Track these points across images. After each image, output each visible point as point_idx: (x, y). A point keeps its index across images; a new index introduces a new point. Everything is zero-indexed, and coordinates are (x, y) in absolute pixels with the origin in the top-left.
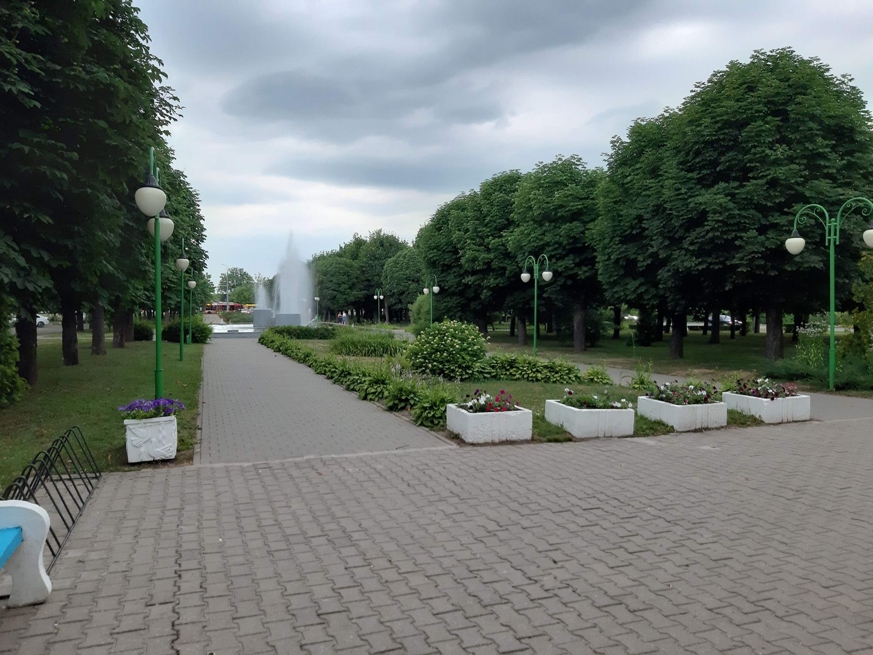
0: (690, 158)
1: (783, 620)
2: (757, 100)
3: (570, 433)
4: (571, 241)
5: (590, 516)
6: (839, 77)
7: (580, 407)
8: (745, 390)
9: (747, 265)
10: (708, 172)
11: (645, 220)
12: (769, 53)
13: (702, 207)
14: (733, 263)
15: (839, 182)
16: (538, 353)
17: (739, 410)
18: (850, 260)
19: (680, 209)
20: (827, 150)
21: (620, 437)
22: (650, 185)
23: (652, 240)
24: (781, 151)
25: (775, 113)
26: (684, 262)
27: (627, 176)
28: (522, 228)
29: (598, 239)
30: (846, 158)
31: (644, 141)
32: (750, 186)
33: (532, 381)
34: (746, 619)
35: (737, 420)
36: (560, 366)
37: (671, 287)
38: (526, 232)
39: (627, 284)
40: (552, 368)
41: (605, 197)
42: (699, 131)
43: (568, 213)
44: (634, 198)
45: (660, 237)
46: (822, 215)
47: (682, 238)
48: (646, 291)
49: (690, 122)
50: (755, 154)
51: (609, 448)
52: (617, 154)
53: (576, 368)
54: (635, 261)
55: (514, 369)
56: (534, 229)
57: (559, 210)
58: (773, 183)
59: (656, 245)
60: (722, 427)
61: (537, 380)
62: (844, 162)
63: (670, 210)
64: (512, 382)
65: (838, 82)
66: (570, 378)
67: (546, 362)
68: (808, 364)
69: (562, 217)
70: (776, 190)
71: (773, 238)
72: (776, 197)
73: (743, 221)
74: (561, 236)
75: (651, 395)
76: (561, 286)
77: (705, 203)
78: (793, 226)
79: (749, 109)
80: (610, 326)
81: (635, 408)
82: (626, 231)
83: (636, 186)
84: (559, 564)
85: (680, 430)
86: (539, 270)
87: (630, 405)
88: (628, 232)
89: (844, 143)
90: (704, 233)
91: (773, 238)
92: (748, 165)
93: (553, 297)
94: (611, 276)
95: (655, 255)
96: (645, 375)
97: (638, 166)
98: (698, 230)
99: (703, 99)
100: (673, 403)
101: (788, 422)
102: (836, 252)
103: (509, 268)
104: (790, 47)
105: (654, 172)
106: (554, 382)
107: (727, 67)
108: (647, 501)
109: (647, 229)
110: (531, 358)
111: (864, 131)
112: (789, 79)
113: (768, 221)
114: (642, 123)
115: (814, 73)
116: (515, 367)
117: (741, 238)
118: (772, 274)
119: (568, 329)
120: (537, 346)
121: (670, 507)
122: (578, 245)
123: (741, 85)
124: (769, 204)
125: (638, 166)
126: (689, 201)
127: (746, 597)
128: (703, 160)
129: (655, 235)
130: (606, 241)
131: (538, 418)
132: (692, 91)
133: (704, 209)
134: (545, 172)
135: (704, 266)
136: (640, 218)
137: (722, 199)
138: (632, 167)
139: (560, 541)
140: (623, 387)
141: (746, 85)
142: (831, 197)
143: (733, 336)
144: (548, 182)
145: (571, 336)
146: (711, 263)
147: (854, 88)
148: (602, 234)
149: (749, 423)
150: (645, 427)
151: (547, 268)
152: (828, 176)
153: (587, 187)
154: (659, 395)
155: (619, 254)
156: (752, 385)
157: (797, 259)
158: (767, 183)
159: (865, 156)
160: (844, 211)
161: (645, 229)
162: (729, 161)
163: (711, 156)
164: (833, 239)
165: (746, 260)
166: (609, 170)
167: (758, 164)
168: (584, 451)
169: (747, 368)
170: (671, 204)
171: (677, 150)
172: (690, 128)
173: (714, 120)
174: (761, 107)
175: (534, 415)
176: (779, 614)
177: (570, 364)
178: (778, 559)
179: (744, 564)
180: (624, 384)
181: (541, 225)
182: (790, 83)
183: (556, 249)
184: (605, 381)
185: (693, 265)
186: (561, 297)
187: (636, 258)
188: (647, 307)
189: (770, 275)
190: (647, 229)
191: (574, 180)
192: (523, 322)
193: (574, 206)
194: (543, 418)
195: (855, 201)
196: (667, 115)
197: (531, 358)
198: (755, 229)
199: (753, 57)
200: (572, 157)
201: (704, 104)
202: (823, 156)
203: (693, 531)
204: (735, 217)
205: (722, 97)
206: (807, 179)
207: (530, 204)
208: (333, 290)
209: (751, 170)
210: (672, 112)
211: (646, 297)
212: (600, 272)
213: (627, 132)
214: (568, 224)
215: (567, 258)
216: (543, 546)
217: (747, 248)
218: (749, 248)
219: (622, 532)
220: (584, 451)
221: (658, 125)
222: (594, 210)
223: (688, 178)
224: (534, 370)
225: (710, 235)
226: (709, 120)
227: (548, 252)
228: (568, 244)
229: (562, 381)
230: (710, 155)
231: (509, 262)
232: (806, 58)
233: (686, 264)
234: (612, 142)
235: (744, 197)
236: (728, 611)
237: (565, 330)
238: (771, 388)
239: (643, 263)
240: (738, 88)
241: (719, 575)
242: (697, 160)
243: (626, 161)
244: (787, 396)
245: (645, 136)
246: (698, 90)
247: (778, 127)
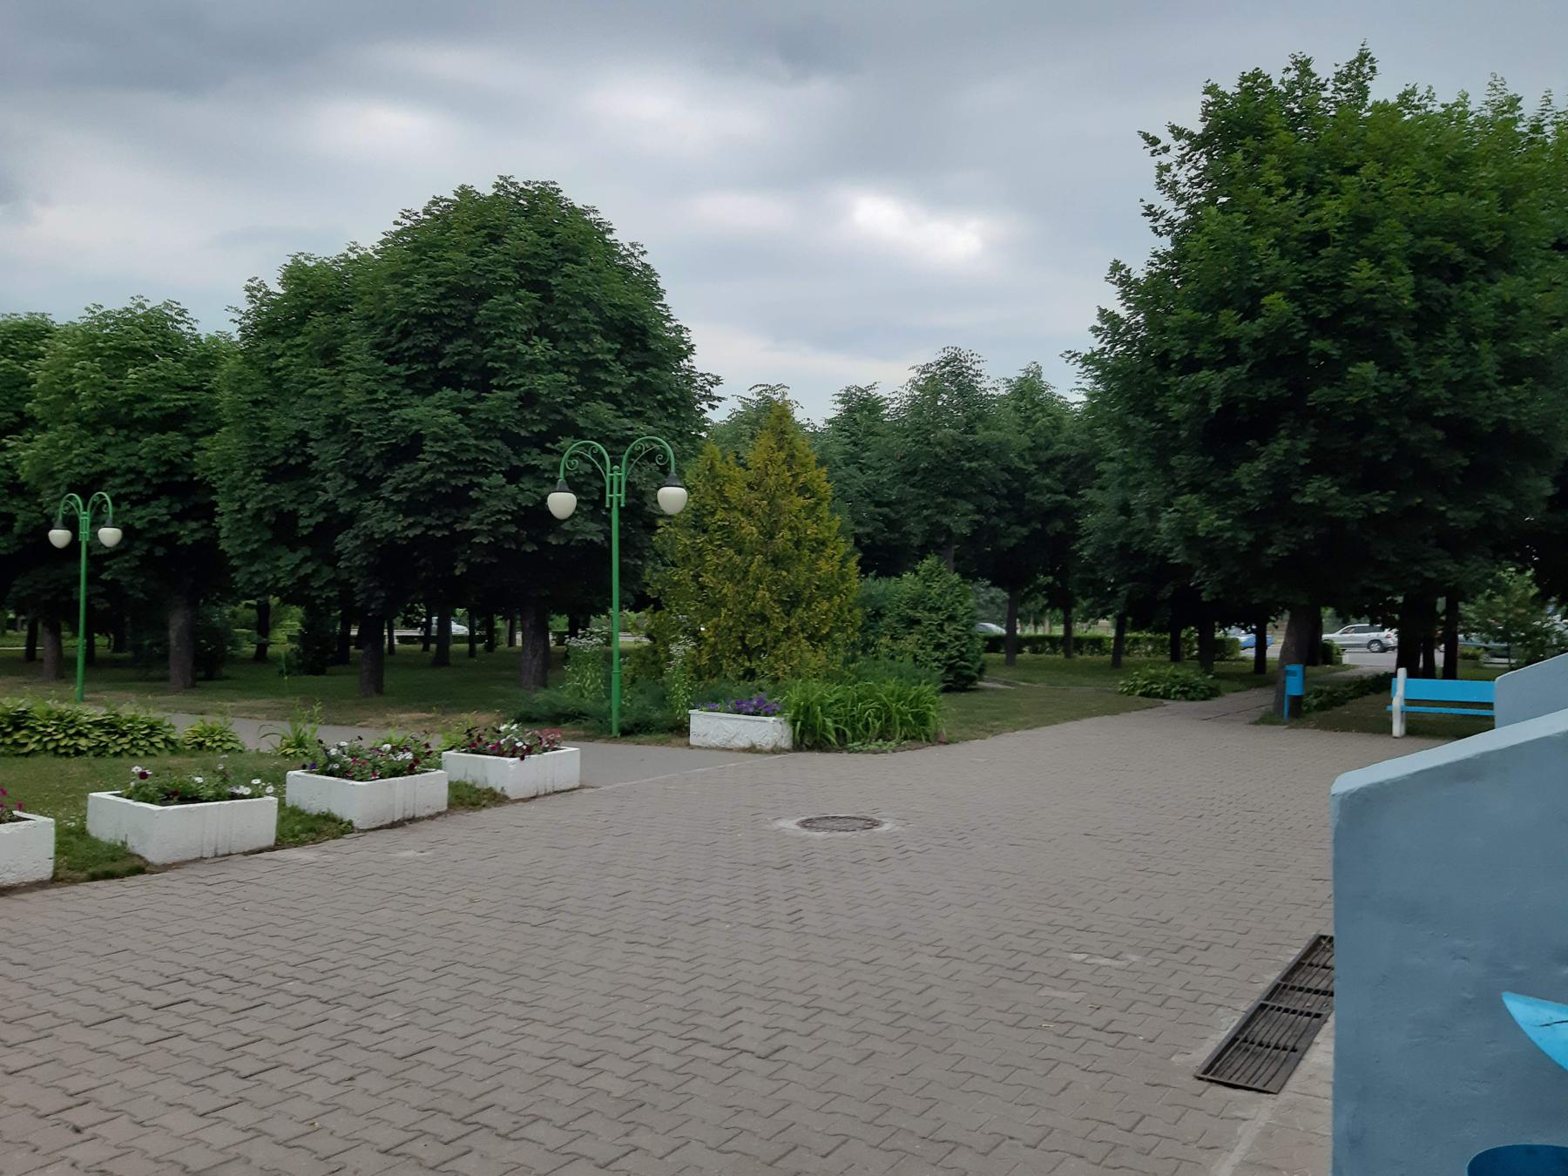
0: (392, 339)
1: (508, 1139)
2: (502, 258)
3: (140, 858)
4: (163, 469)
5: (168, 1020)
6: (627, 246)
7: (163, 802)
8: (479, 745)
9: (489, 533)
10: (425, 368)
11: (312, 440)
12: (522, 185)
13: (415, 427)
14: (465, 528)
15: (626, 409)
16: (86, 696)
17: (469, 782)
18: (643, 531)
19: (375, 428)
20: (609, 357)
21: (246, 854)
22: (321, 378)
23: (324, 479)
24: (540, 349)
25: (534, 286)
26: (382, 522)
27: (279, 357)
28: (51, 434)
29: (221, 469)
30: (635, 373)
31: (311, 297)
32: (494, 399)
33: (67, 755)
34: (635, 1049)
35: (466, 798)
36: (130, 721)
37: (360, 567)
38: (62, 443)
39: (278, 558)
40: (112, 726)
41: (235, 390)
42: (408, 294)
43: (157, 414)
44: (293, 400)
45: (339, 474)
46: (601, 458)
47: (380, 480)
48: (315, 572)
49: (394, 275)
50: (501, 348)
51: (222, 878)
52: (259, 313)
53: (167, 724)
54: (294, 515)
55: (24, 732)
56: (80, 440)
57: (137, 406)
58: (529, 399)
59: (332, 489)
60: (439, 814)
61: (78, 753)
62: (633, 379)
63: (359, 426)
64: (17, 760)
65: (624, 253)
66: (152, 744)
67: (98, 713)
68: (582, 696)
69: (141, 420)
70: (534, 412)
71: (529, 490)
72: (534, 422)
73: (481, 458)
74: (141, 458)
75: (312, 767)
77: (420, 421)
78: (558, 472)
79: (490, 271)
80: (249, 638)
81: (280, 795)
82: (276, 458)
83: (295, 377)
84: (87, 1134)
85: (365, 828)
86: (92, 525)
87: (270, 789)
88: (281, 461)
89: (634, 350)
90: (417, 473)
91: (529, 490)
92: (490, 364)
93: (124, 580)
94: (245, 543)
95: (329, 507)
96: (307, 730)
97: (299, 340)
98: (407, 467)
99: (415, 241)
100: (352, 778)
101: (547, 795)
102: (621, 517)
103: (21, 517)
104: (554, 183)
105: (329, 355)
106: (116, 754)
107: (456, 193)
108: (286, 971)
109: (316, 458)
110: (64, 707)
111: (660, 335)
112: (552, 235)
113: (522, 461)
114: (307, 262)
115: (590, 233)
116: (27, 728)
117: (479, 485)
118: (529, 550)
119: (158, 645)
120: (86, 680)
121: (330, 974)
122: (179, 479)
123: (478, 228)
124: (523, 433)
125: (299, 340)
126: (391, 414)
127: (449, 1114)
128: (415, 346)
129: (332, 470)
130: (239, 473)
131: (70, 832)
132: (396, 223)
133: (417, 431)
134: (107, 326)
135: (418, 531)
136: (303, 437)
137: (447, 418)
138: (289, 341)
139: (94, 1083)
140: (262, 756)
141: (486, 231)
142: (614, 431)
143: (472, 652)
144: (111, 348)
145: (164, 657)
146: (429, 527)
147: (647, 266)
148: (227, 460)
149: (484, 802)
150: (298, 827)
151: (109, 522)
152: (610, 398)
153: (199, 367)
154: (326, 765)
155: (262, 502)
156: (492, 737)
157: (566, 526)
158: (520, 398)
159: (663, 374)
160: (632, 456)
161: (311, 458)
162: (459, 354)
163: (429, 341)
164: (616, 498)
165: (488, 524)
166: (242, 340)
167: (504, 365)
168: (168, 891)
169: (489, 707)
170: (358, 417)
171: (371, 323)
172: (392, 286)
173: (432, 280)
174: (508, 271)
175: (57, 826)
176: (502, 1131)
177: (155, 715)
178: (509, 1032)
179: (453, 1053)
180: (265, 748)
181: (97, 432)
182: (556, 241)
183: (129, 483)
184: (228, 745)
185: (399, 528)
186: (143, 580)
187: (295, 511)
188: (318, 602)
189: (525, 552)
190: (316, 458)
191: (171, 351)
192: (56, 632)
193: (169, 401)
194: (82, 833)
195: (648, 440)
196: (353, 256)
197: (64, 707)
198: (501, 472)
199: (497, 185)
200: (167, 305)
201: (415, 250)
202: (602, 366)
203: (370, 1011)
204: (469, 450)
205: (447, 244)
206: (580, 399)
207: (71, 387)
209: (495, 372)
210: (362, 253)
211: (315, 584)
212: (223, 533)
213: (279, 274)
214: (156, 435)
215: (154, 503)
216: (50, 1101)
217: (488, 504)
218: (493, 504)
219: (230, 1040)
220: (168, 891)
221: (338, 272)
222: (214, 412)
223: (390, 375)
224: (71, 732)
225: (428, 477)
226: (424, 279)
227: (113, 487)
228: (156, 475)
229: (134, 751)
230: (426, 338)
231: (23, 504)
232: (578, 205)
233: (385, 526)
234: (248, 289)
235: (484, 417)
236: (417, 1148)
237: (151, 646)
238: (521, 740)
239: (307, 522)
240: (472, 233)
241: (407, 1084)
242: (404, 345)
243: (276, 327)
244: (545, 750)
245: (312, 288)
246: (408, 223)
247: (537, 309)
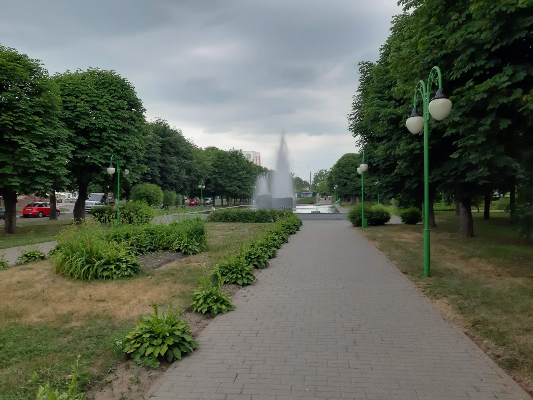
76: (487, 134)
151: (413, 111)
208: (344, 178)
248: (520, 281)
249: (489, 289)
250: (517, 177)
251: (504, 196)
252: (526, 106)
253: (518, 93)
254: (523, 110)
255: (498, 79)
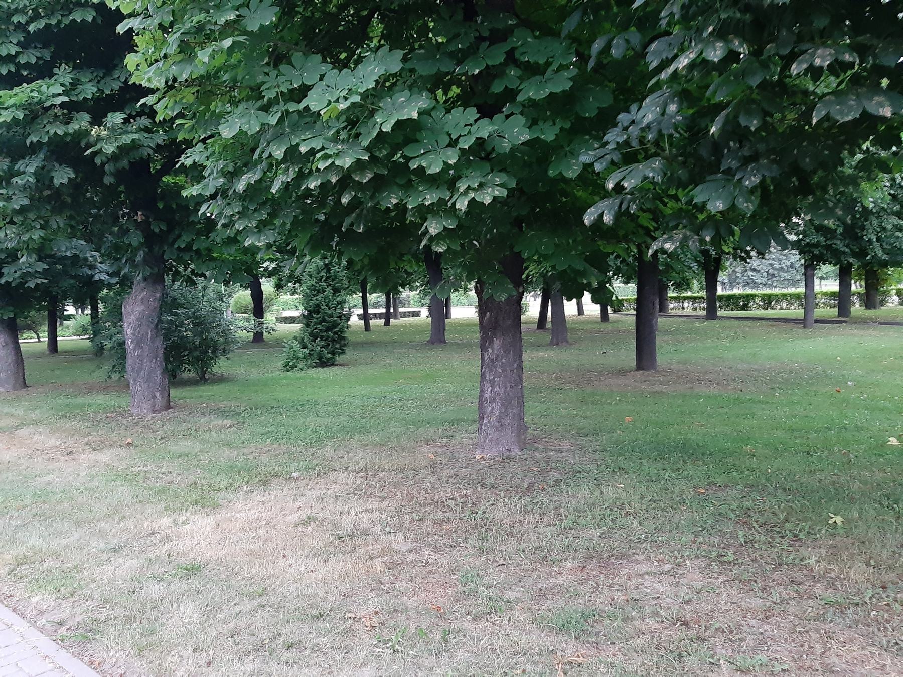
248: (105, 457)
249: (49, 483)
250: (97, 278)
251: (83, 313)
252: (98, 147)
253: (82, 121)
254: (95, 154)
255: (44, 88)
